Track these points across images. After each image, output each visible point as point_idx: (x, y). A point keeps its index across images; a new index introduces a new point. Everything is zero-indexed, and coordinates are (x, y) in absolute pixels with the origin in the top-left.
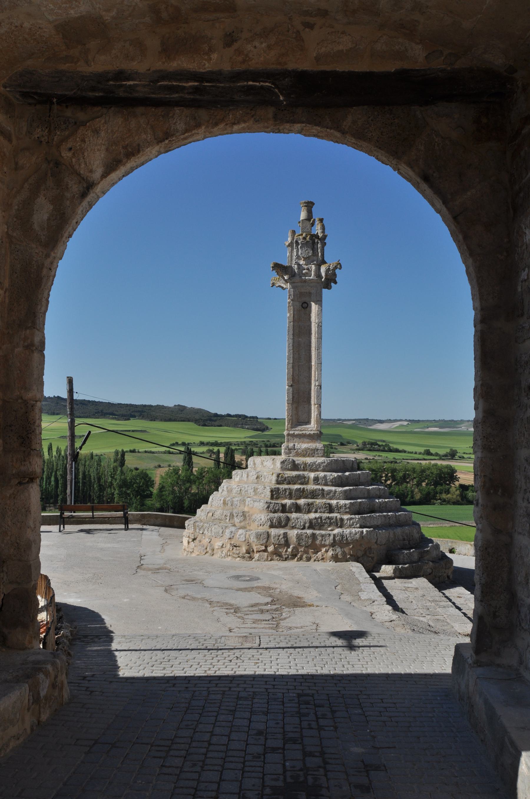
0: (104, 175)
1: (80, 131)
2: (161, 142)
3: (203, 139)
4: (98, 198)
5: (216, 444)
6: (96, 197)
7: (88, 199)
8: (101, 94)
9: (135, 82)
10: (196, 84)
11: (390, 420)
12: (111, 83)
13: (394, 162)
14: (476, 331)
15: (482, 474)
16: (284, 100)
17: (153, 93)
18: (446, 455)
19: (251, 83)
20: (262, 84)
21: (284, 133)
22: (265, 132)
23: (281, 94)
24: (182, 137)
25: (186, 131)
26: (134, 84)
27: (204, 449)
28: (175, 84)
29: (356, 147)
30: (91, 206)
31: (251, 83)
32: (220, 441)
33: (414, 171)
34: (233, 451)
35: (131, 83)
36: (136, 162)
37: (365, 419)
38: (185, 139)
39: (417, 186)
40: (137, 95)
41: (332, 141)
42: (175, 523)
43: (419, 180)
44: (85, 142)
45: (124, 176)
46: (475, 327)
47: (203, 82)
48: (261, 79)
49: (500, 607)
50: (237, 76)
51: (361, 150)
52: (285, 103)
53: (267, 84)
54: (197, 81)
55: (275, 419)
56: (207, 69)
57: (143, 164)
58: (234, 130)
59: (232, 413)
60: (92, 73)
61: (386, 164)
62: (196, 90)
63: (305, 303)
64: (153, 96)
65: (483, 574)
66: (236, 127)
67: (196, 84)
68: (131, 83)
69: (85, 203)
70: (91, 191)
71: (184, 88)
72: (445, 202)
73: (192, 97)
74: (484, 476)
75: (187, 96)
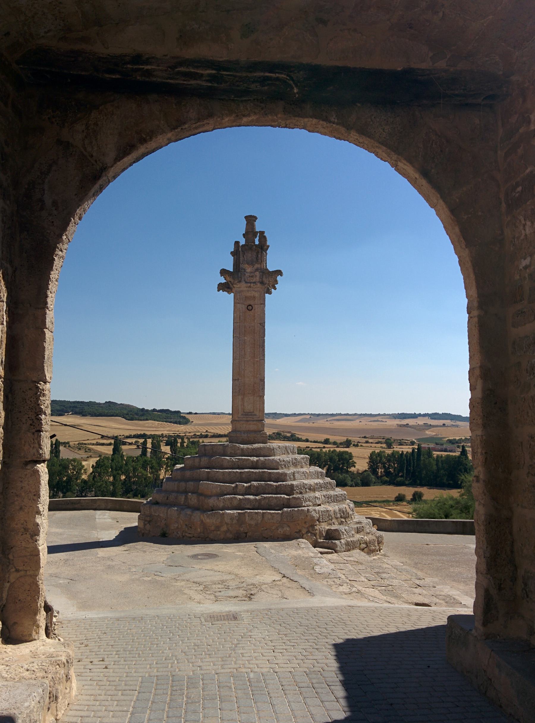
0: (118, 159)
1: (92, 114)
2: (174, 129)
3: (212, 130)
4: (109, 182)
5: (143, 436)
6: (107, 181)
7: (100, 182)
8: (118, 76)
9: (153, 67)
10: (214, 72)
11: (295, 414)
12: (129, 66)
13: (395, 157)
14: (470, 318)
15: (483, 452)
16: (297, 93)
17: (171, 79)
18: (341, 444)
19: (267, 74)
20: (277, 75)
21: (290, 128)
22: (272, 126)
23: (296, 86)
24: (194, 126)
25: (199, 120)
26: (152, 69)
27: (133, 440)
28: (192, 70)
29: (358, 144)
30: (101, 189)
31: (267, 74)
32: (148, 433)
33: (413, 166)
34: (159, 442)
35: (149, 67)
36: (147, 148)
37: (273, 413)
38: (196, 128)
39: (413, 182)
40: (155, 79)
41: (335, 137)
42: (125, 507)
43: (417, 175)
44: (97, 125)
45: (134, 162)
46: (469, 313)
47: (220, 71)
48: (277, 71)
49: (505, 580)
50: (254, 66)
51: (363, 147)
52: (297, 96)
53: (283, 76)
54: (213, 69)
55: (196, 413)
56: (225, 59)
57: (153, 151)
58: (243, 122)
59: (158, 409)
60: (109, 55)
61: (385, 161)
62: (213, 78)
63: (250, 305)
64: (172, 81)
65: (487, 547)
66: (245, 120)
67: (214, 72)
68: (149, 67)
69: (97, 186)
70: (104, 174)
71: (202, 75)
72: (443, 197)
73: (210, 84)
74: (486, 453)
75: (204, 84)
